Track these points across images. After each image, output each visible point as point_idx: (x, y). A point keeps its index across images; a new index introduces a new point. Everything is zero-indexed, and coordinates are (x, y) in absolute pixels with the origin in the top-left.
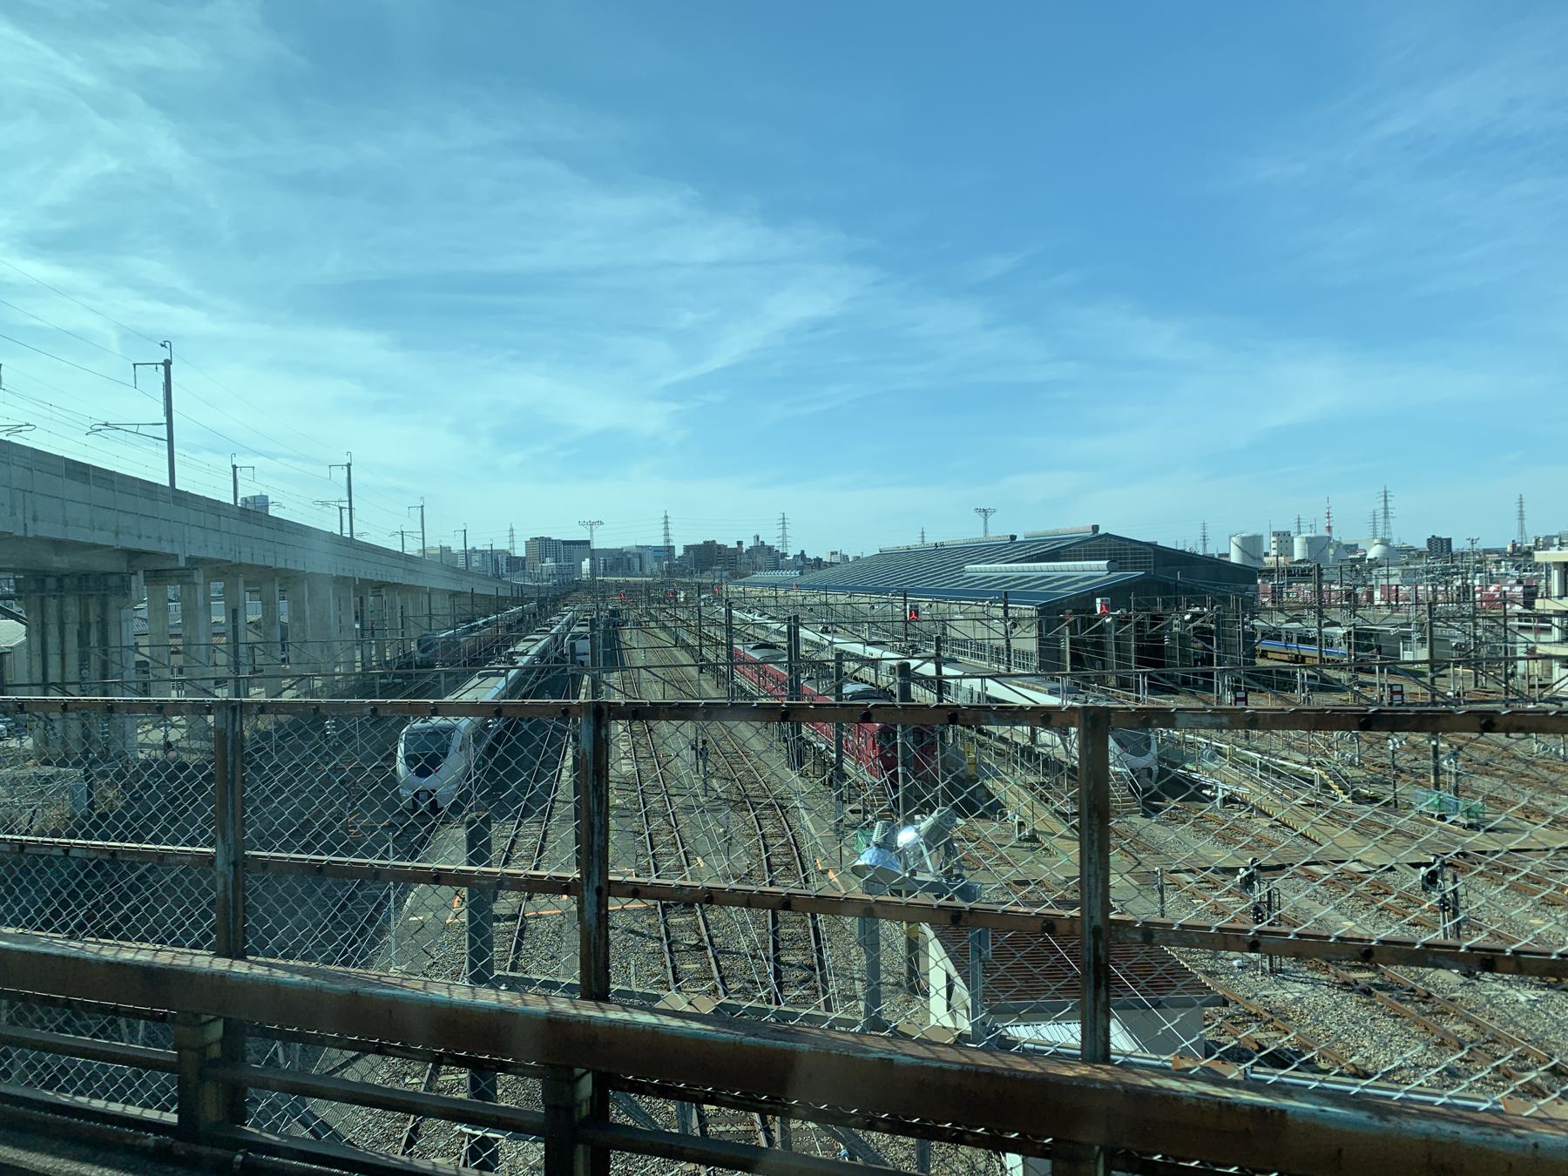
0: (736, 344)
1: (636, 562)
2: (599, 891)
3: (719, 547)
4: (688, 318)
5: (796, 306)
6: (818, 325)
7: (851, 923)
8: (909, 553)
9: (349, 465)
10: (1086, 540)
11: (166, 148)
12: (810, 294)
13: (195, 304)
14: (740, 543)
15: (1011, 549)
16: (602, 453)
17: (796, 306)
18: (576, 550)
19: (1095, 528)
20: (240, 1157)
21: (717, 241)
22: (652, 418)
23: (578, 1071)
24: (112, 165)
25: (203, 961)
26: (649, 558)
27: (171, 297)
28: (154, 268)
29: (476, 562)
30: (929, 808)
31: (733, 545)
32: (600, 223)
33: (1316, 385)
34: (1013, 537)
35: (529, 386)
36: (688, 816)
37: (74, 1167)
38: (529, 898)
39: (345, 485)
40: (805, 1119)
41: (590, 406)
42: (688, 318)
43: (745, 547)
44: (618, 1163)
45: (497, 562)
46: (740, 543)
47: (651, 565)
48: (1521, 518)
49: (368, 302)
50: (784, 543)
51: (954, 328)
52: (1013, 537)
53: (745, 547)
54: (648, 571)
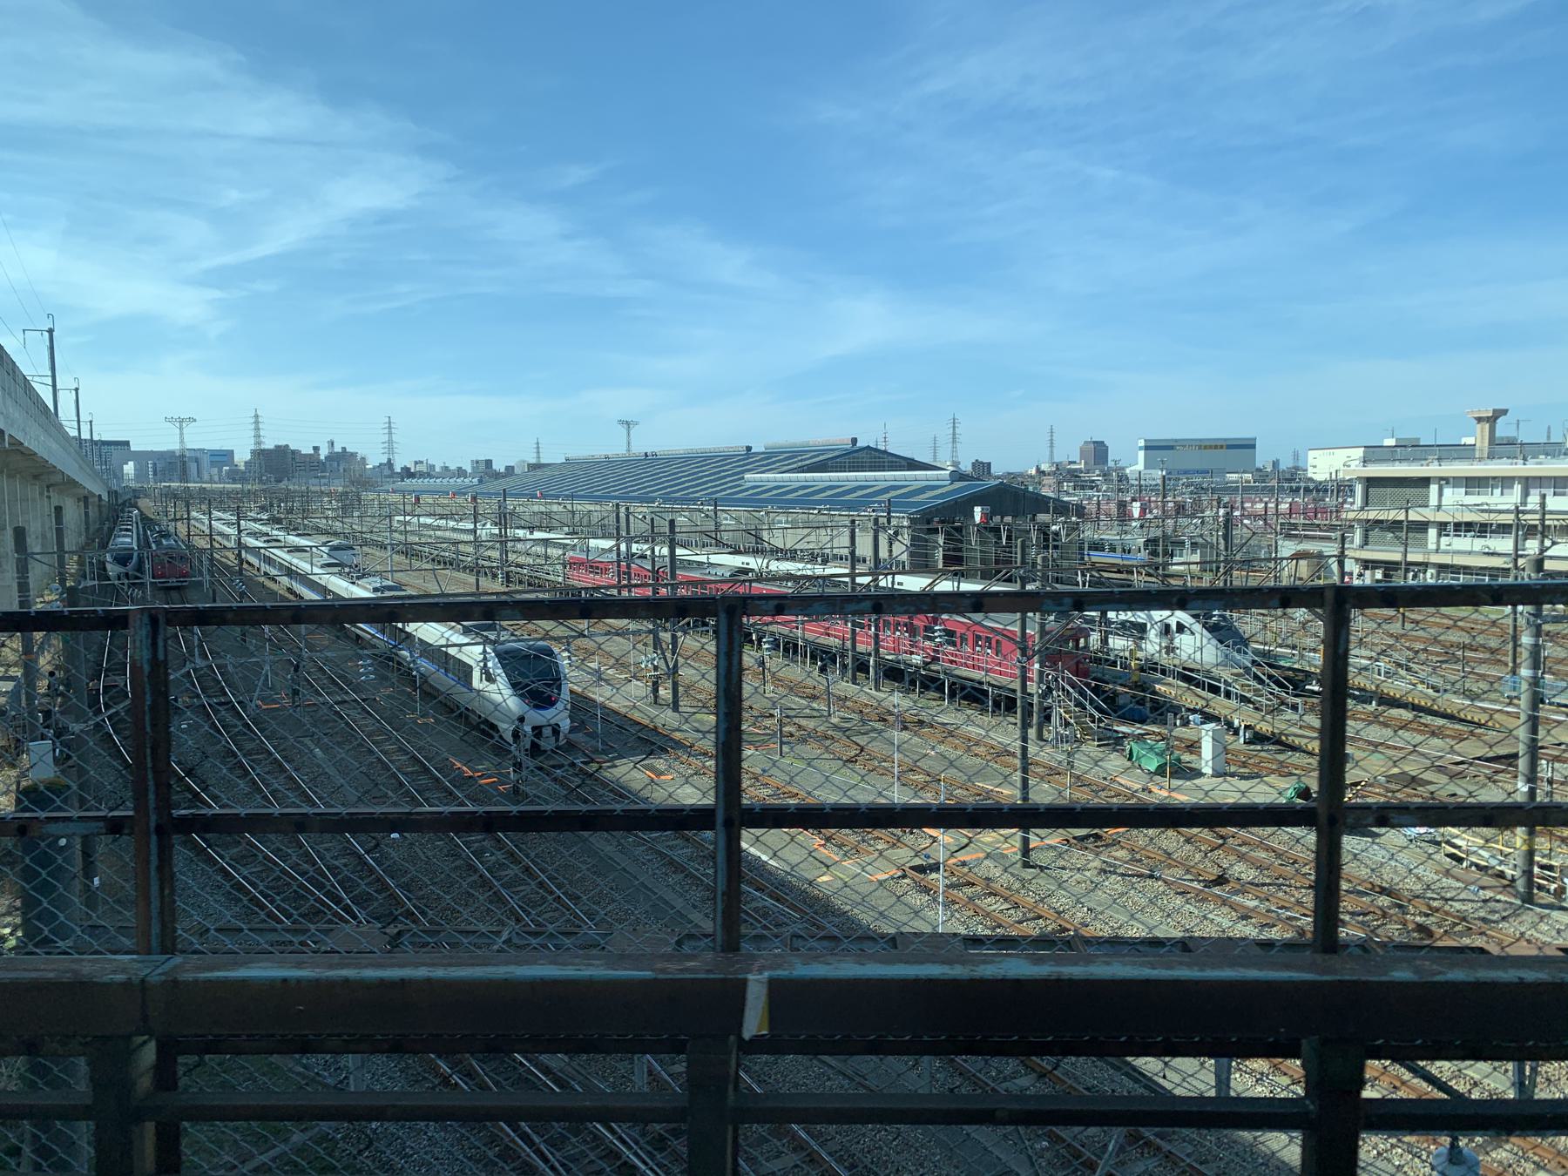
0: (287, 232)
1: (193, 467)
3: (293, 452)
4: (233, 195)
7: (1362, 854)
8: (608, 462)
9: (77, 390)
10: (848, 453)
12: (372, 184)
14: (316, 449)
15: (772, 459)
18: (116, 453)
21: (266, 114)
22: (188, 305)
26: (206, 461)
30: (52, 692)
33: (866, 320)
38: (115, 827)
42: (233, 195)
44: (1371, 1146)
46: (316, 449)
47: (210, 471)
48: (954, 440)
50: (390, 446)
51: (531, 234)
52: (749, 449)
54: (206, 477)
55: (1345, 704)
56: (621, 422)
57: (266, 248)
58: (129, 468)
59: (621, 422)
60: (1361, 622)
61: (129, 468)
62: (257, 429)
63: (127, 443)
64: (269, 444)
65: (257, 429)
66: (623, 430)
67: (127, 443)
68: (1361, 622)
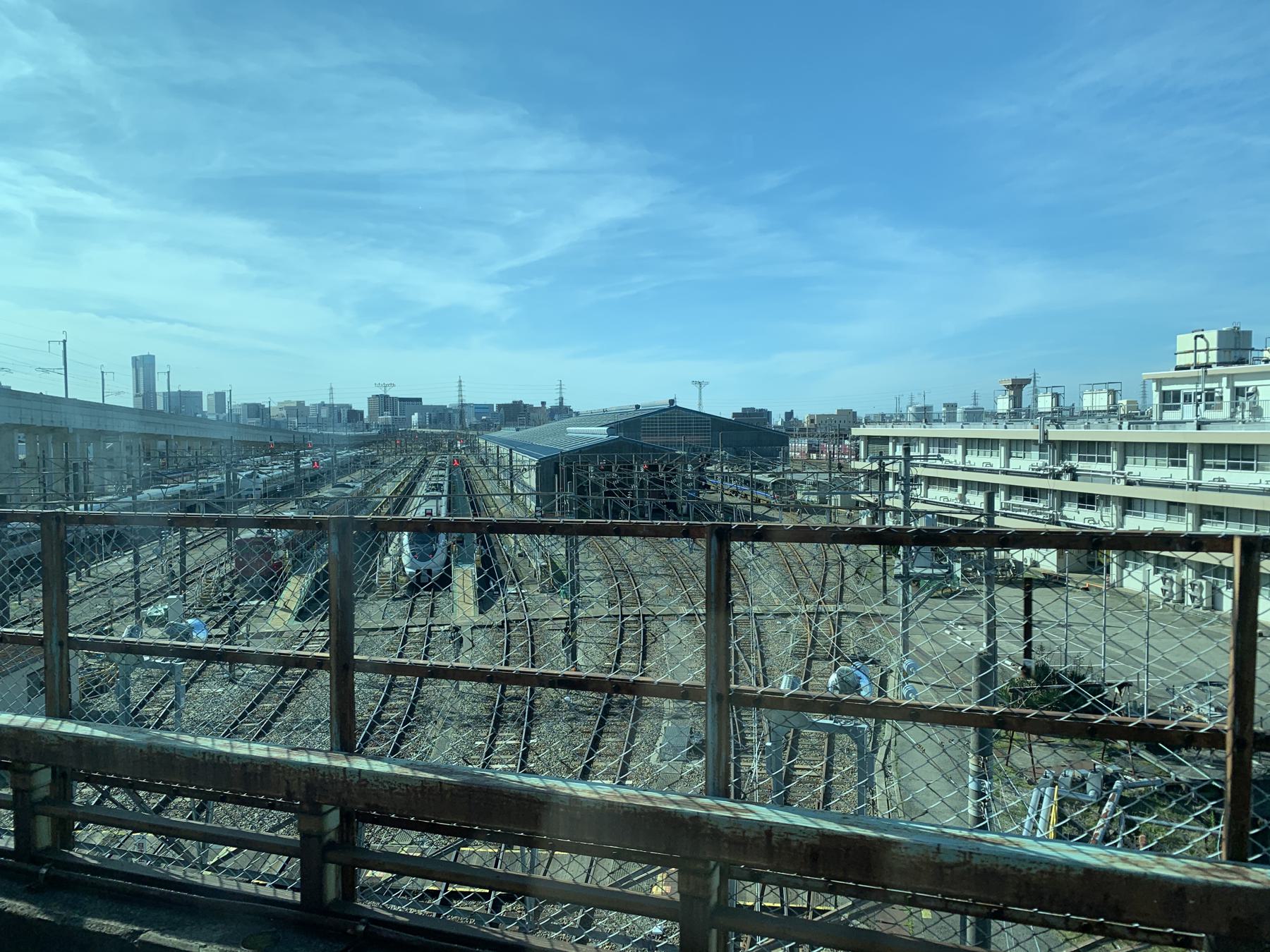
0: (557, 238)
2: (61, 644)
3: (525, 406)
4: (519, 214)
5: (611, 207)
6: (625, 225)
9: (65, 342)
11: (74, 57)
13: (102, 192)
14: (543, 403)
16: (445, 325)
17: (611, 207)
18: (407, 406)
19: (672, 402)
20: (44, 871)
21: (543, 152)
22: (488, 298)
23: (326, 808)
24: (28, 70)
25: (36, 722)
27: (80, 184)
28: (66, 161)
29: (324, 414)
31: (537, 404)
32: (440, 136)
34: (638, 407)
35: (386, 268)
36: (129, 599)
37: (171, 941)
39: (61, 354)
40: (184, 796)
41: (442, 287)
43: (548, 406)
45: (339, 414)
46: (543, 403)
49: (242, 194)
53: (548, 406)
55: (16, 824)
56: (694, 383)
57: (539, 254)
58: (415, 418)
59: (694, 383)
60: (1039, 594)
61: (415, 418)
62: (460, 390)
63: (420, 400)
64: (174, 389)
65: (460, 390)
66: (696, 389)
67: (420, 400)
68: (1039, 594)
